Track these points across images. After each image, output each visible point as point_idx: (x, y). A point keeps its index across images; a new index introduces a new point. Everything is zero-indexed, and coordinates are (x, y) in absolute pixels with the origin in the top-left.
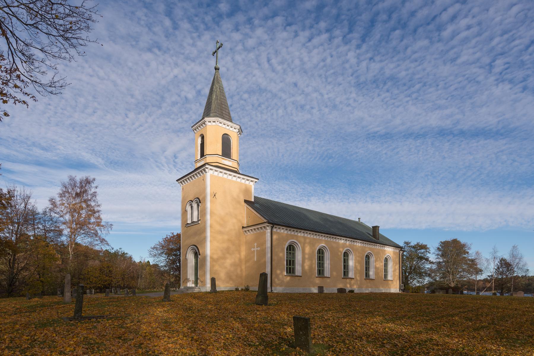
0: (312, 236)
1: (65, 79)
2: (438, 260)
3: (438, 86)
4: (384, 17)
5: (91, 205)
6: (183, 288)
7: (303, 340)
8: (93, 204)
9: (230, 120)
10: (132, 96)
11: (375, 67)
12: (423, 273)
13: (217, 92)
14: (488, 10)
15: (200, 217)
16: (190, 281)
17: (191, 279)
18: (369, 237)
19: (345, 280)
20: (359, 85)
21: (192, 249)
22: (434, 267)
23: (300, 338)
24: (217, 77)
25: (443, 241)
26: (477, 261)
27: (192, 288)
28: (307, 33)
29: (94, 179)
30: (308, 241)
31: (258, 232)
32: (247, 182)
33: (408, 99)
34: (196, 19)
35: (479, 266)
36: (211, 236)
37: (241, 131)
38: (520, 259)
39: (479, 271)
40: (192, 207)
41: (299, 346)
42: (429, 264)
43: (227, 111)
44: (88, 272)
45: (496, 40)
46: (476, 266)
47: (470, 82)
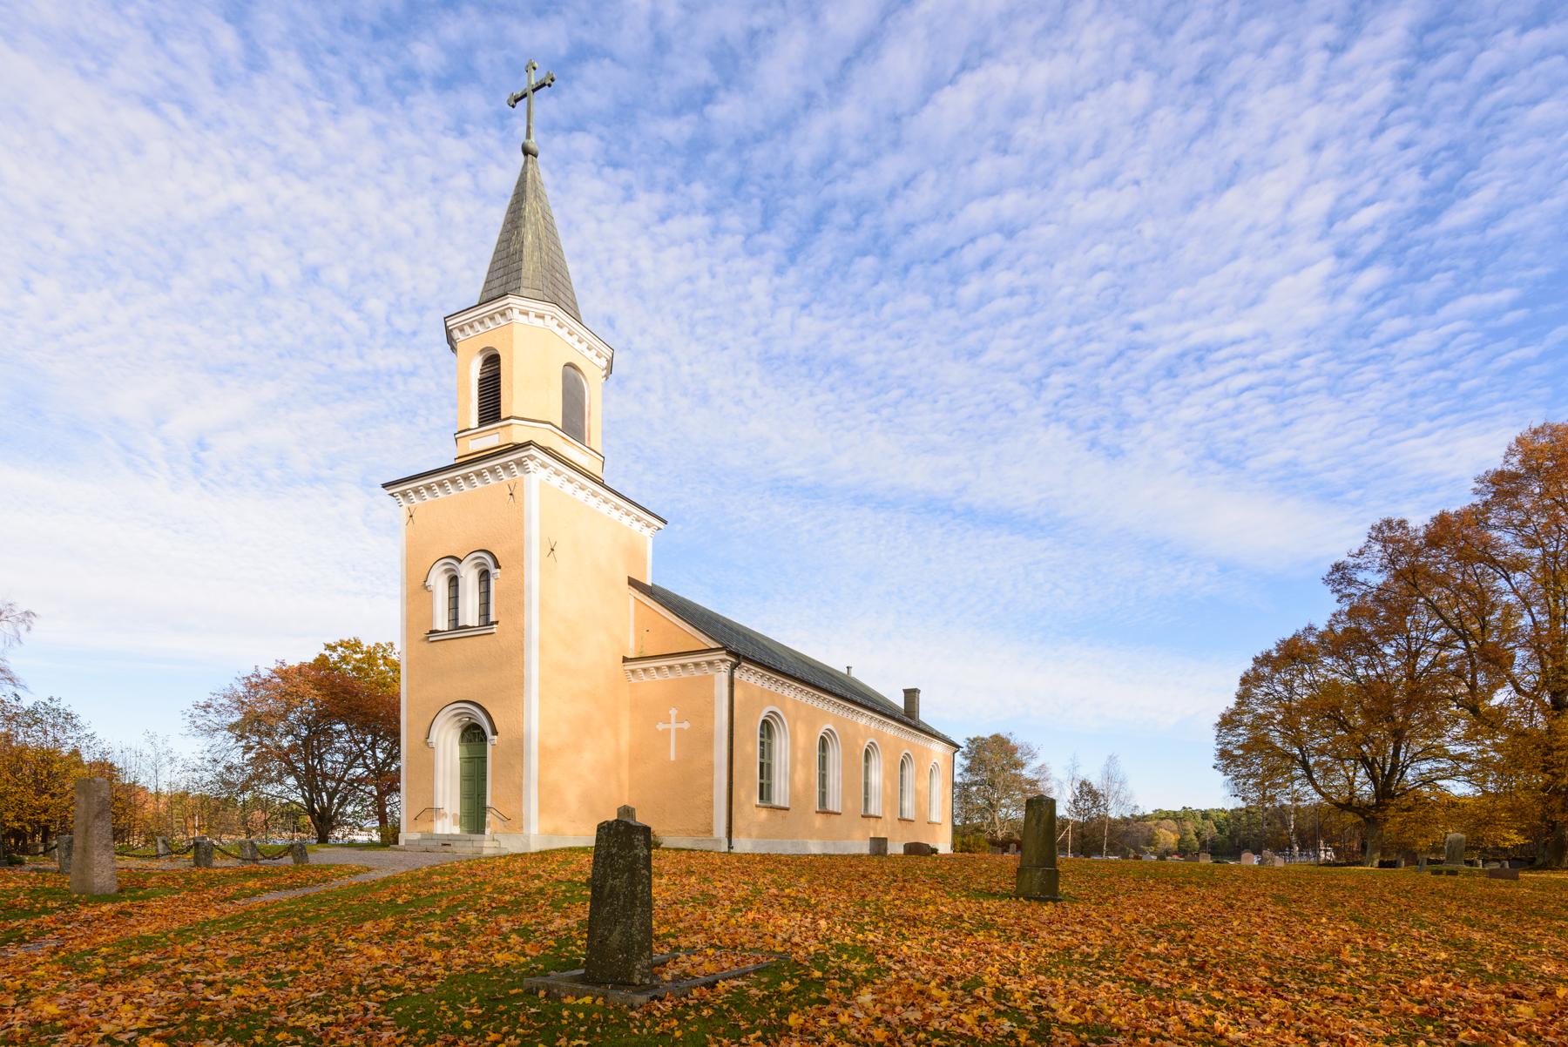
3: (936, 402)
4: (844, 217)
10: (61, 229)
11: (810, 326)
13: (536, 224)
14: (1052, 266)
16: (445, 815)
17: (447, 810)
19: (866, 820)
20: (771, 361)
28: (658, 200)
31: (658, 677)
32: (637, 526)
33: (874, 416)
34: (330, 60)
36: (542, 680)
45: (1060, 332)
47: (998, 408)
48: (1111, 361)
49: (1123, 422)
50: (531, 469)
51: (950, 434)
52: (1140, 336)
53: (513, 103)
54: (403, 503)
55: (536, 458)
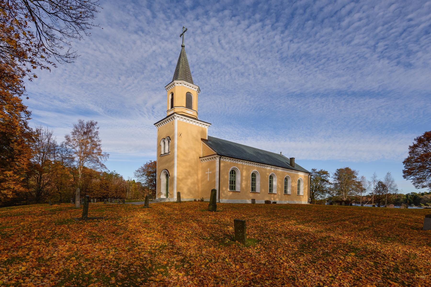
0: (248, 164)
1: (76, 52)
2: (335, 182)
3: (337, 60)
4: (301, 11)
8: (95, 140)
9: (192, 83)
11: (294, 46)
12: (324, 190)
14: (374, 7)
17: (163, 193)
18: (287, 165)
20: (282, 59)
22: (332, 186)
26: (362, 183)
28: (247, 22)
29: (97, 123)
30: (245, 167)
32: (203, 126)
33: (317, 69)
34: (169, 11)
35: (363, 187)
37: (199, 90)
38: (392, 182)
39: (363, 190)
40: (164, 143)
41: (237, 240)
43: (190, 76)
45: (380, 28)
47: (360, 58)
48: (401, 34)
49: (409, 53)
51: (344, 70)
52: (412, 23)
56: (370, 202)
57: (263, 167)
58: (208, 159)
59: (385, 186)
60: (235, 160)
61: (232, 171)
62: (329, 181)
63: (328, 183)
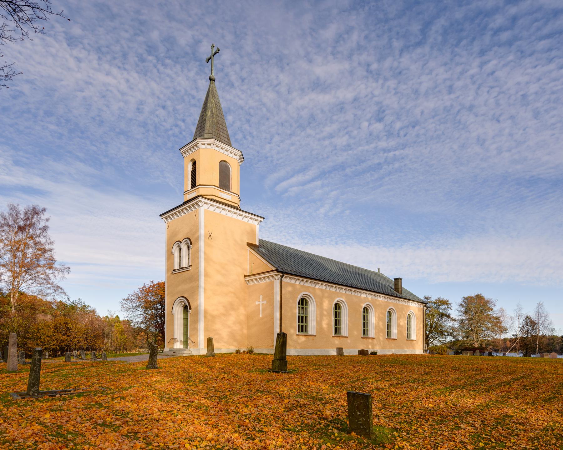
0: (331, 289)
1: (12, 66)
2: (461, 317)
5: (41, 243)
6: (168, 350)
7: (360, 422)
8: (43, 240)
9: (230, 144)
12: (444, 331)
13: (212, 108)
15: (192, 262)
17: (178, 339)
18: (391, 290)
21: (180, 302)
22: (456, 325)
23: (357, 421)
24: (213, 89)
25: (466, 296)
26: (502, 319)
27: (180, 350)
29: (44, 210)
30: (326, 294)
32: (251, 221)
35: (503, 325)
37: (242, 158)
38: (546, 317)
39: (503, 330)
40: (180, 249)
41: (354, 430)
42: (451, 321)
43: (225, 132)
44: (38, 329)
46: (501, 324)
50: (200, 206)
53: (207, 61)
54: (166, 222)
55: (202, 201)
56: (514, 350)
57: (356, 294)
58: (268, 277)
59: (534, 323)
60: (307, 281)
61: (302, 299)
62: (452, 316)
63: (450, 320)
